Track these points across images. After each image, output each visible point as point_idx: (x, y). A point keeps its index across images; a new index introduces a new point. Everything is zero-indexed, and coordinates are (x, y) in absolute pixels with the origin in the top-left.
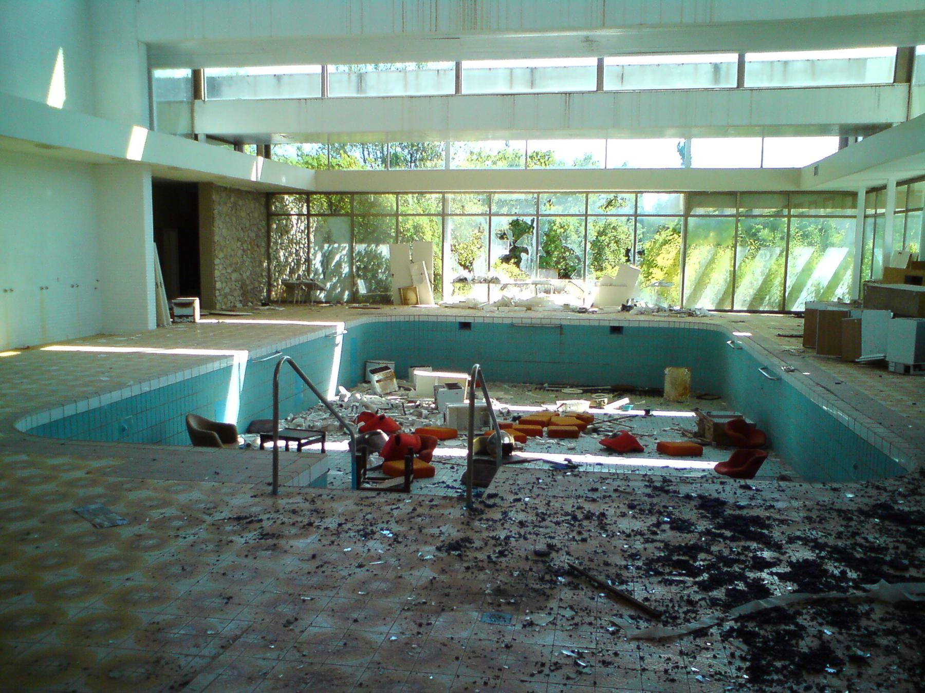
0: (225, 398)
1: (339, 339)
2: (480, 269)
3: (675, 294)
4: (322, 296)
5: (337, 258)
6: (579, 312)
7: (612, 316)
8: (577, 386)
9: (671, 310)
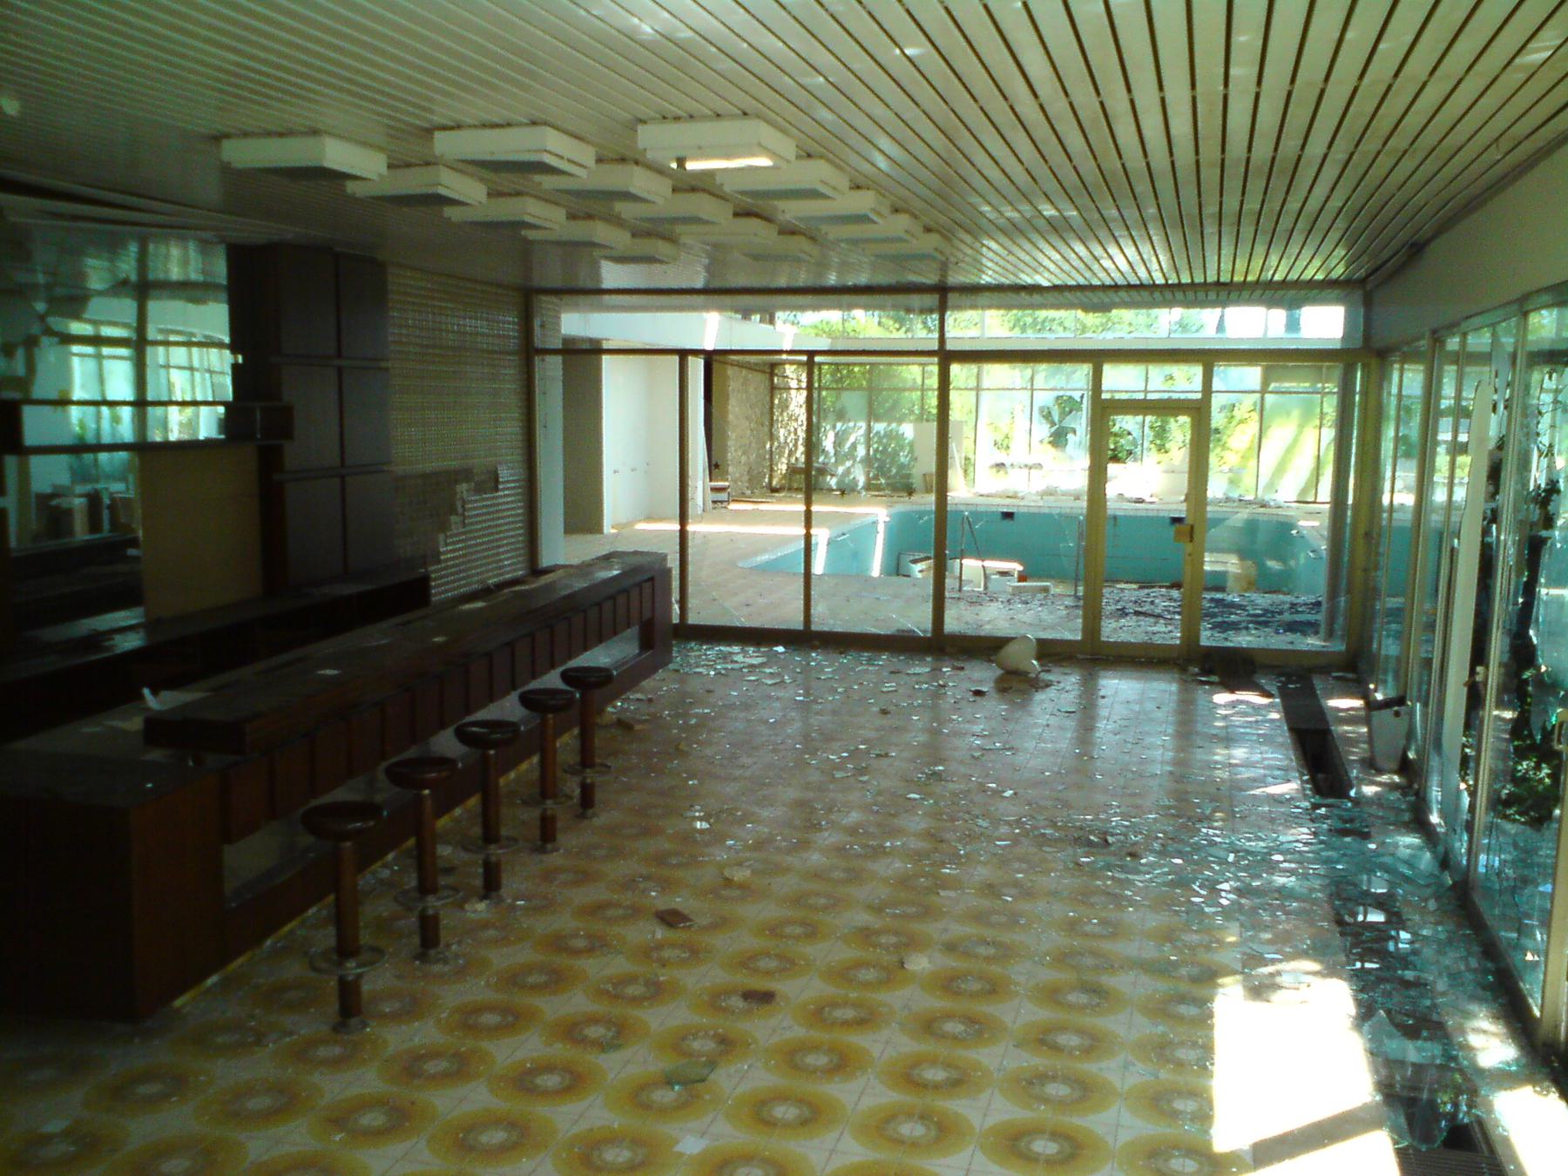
0: (884, 549)
1: (881, 528)
2: (1018, 454)
3: (1248, 481)
4: (833, 482)
5: (852, 439)
6: (1136, 502)
7: (1174, 507)
8: (1135, 583)
9: (1241, 500)
